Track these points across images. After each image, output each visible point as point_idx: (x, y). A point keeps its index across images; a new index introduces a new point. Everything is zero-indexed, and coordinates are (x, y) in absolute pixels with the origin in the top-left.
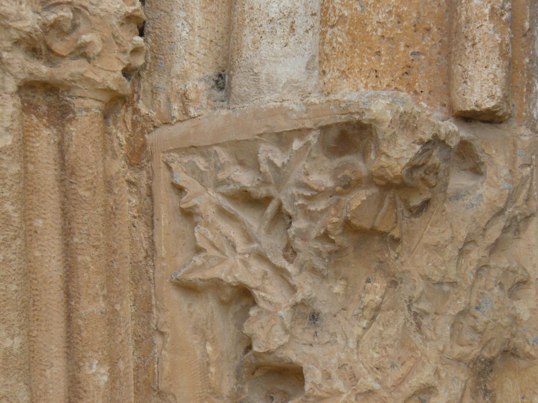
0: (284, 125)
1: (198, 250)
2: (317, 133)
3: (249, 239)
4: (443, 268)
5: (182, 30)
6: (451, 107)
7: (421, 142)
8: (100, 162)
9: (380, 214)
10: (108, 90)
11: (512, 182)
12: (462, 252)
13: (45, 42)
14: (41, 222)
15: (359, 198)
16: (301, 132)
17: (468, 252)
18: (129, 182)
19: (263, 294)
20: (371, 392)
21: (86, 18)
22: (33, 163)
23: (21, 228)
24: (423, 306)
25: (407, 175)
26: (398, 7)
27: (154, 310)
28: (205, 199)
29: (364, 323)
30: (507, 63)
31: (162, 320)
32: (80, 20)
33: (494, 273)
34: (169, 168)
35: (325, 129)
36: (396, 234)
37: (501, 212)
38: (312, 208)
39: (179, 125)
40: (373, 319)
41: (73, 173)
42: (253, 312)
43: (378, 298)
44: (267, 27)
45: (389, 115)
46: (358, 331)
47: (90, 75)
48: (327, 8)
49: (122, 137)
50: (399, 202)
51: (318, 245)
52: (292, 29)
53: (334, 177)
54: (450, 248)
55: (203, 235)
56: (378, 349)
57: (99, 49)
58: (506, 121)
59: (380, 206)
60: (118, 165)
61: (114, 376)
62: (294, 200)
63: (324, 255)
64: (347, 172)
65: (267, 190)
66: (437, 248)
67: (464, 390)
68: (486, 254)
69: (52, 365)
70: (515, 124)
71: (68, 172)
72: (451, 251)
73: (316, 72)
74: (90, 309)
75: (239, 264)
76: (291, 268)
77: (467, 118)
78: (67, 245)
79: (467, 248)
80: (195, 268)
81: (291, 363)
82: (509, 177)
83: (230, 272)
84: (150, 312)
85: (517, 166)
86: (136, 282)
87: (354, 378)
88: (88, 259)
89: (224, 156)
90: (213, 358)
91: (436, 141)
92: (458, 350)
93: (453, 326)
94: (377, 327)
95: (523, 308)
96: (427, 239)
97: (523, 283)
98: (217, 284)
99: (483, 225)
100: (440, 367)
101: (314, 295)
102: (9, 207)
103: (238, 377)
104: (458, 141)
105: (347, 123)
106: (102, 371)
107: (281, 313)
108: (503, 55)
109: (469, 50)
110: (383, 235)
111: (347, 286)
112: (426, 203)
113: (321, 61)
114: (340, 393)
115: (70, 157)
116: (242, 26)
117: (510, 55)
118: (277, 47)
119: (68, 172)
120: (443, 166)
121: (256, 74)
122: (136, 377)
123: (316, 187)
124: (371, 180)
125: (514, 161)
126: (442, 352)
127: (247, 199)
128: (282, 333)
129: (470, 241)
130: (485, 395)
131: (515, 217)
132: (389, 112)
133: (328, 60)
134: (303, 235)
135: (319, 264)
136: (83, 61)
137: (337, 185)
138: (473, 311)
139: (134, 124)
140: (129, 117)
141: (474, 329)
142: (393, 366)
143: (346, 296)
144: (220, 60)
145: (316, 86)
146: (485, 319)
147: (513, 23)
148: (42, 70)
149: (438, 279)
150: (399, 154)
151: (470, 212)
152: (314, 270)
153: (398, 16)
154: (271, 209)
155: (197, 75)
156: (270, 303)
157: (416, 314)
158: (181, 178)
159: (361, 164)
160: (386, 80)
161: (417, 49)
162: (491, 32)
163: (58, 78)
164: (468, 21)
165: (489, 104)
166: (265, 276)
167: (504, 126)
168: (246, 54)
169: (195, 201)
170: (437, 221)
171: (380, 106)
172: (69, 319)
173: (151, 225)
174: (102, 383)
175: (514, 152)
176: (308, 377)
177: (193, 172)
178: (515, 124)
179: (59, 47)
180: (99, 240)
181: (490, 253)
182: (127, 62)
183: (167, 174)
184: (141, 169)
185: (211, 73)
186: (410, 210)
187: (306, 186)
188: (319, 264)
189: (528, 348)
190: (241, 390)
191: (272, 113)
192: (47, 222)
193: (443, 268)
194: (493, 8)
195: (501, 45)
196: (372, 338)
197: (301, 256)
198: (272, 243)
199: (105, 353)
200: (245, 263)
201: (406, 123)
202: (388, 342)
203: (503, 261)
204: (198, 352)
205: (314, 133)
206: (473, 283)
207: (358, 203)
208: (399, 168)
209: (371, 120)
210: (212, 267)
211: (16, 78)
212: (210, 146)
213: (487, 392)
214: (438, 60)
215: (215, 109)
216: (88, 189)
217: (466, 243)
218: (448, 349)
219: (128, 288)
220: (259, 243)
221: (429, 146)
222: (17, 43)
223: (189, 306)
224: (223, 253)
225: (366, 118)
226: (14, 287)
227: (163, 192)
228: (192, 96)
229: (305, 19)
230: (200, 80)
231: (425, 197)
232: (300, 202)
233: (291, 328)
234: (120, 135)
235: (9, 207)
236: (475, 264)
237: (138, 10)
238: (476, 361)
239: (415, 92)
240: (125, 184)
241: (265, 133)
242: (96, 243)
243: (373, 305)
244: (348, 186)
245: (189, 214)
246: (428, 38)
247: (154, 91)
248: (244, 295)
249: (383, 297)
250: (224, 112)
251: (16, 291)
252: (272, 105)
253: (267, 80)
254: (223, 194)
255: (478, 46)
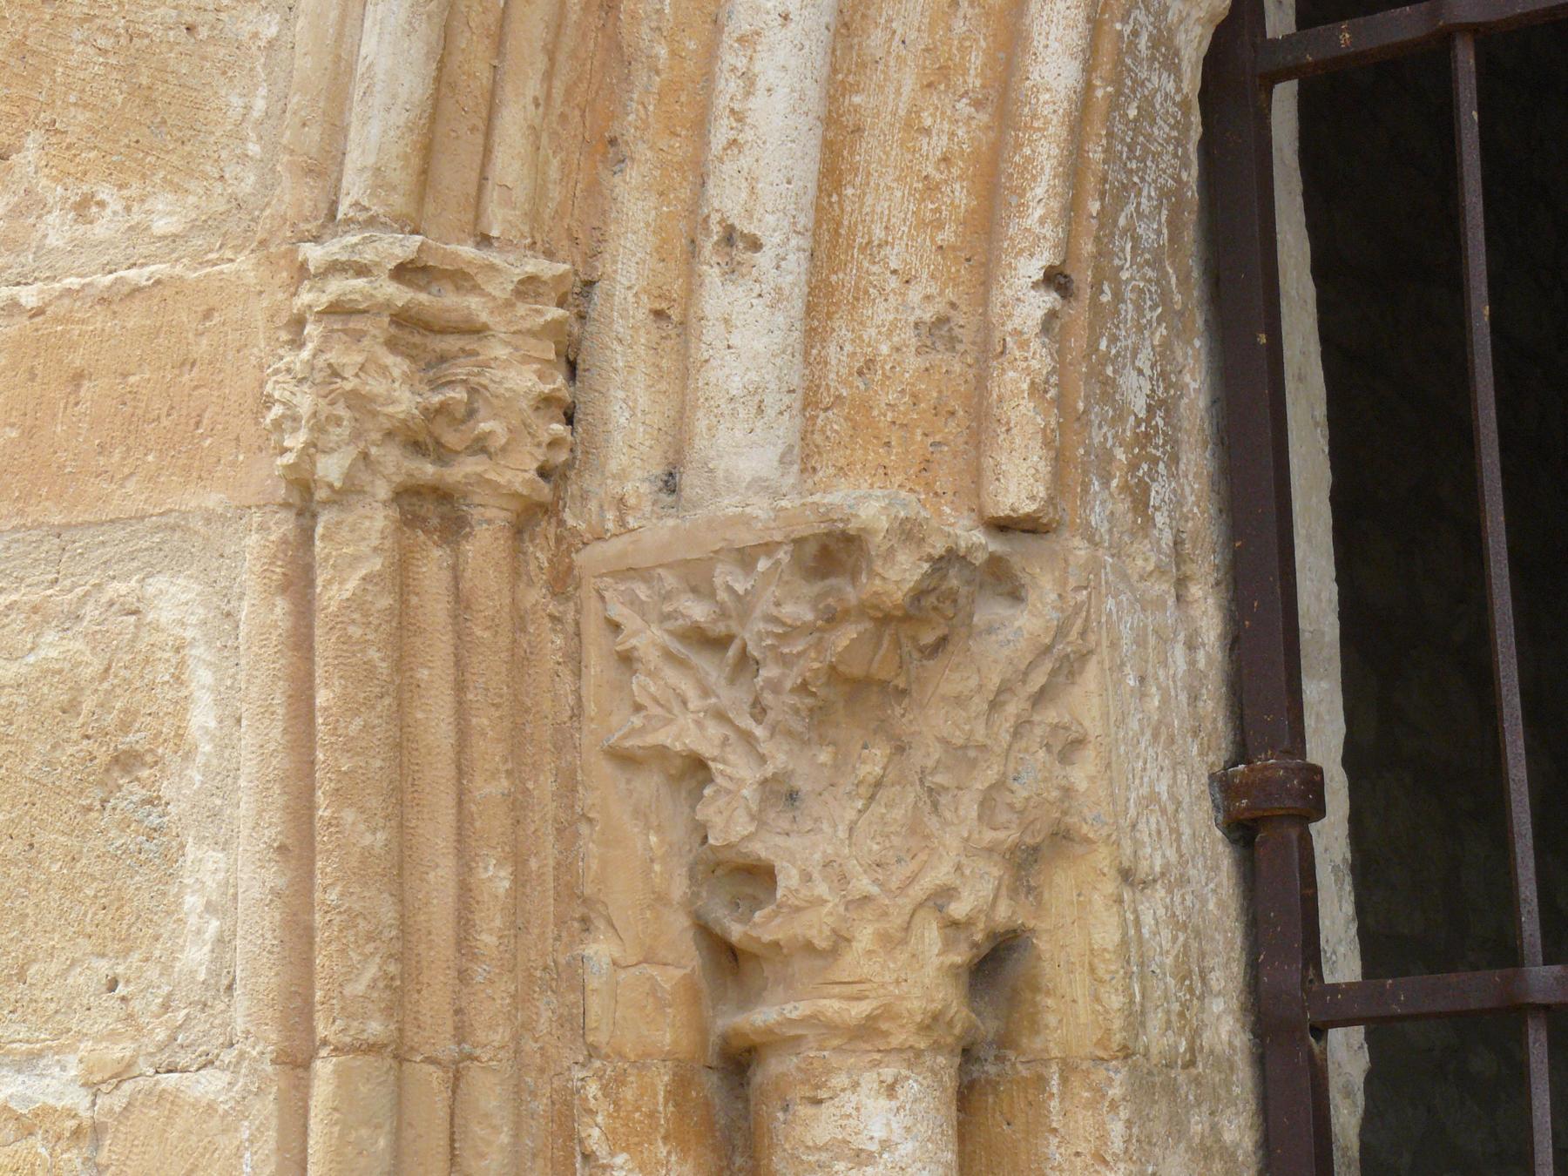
0: (747, 538)
1: (638, 708)
2: (789, 548)
3: (706, 692)
4: (967, 727)
5: (619, 416)
6: (981, 512)
7: (930, 558)
8: (506, 592)
9: (878, 658)
10: (515, 495)
11: (1062, 610)
12: (995, 705)
13: (430, 434)
14: (426, 672)
15: (845, 637)
16: (768, 548)
17: (1004, 703)
18: (552, 617)
19: (721, 767)
20: (867, 899)
21: (486, 400)
22: (417, 594)
23: (392, 682)
24: (939, 779)
25: (912, 604)
26: (913, 385)
27: (580, 788)
28: (647, 638)
29: (860, 804)
30: (1052, 454)
31: (589, 802)
32: (479, 404)
33: (1038, 731)
34: (602, 598)
35: (799, 542)
36: (901, 683)
37: (1048, 649)
38: (786, 650)
39: (614, 540)
40: (872, 797)
41: (468, 607)
42: (708, 791)
43: (878, 770)
44: (726, 408)
45: (884, 524)
46: (850, 815)
47: (491, 476)
48: (818, 386)
49: (543, 557)
50: (904, 640)
51: (793, 700)
52: (760, 410)
53: (815, 608)
54: (976, 699)
55: (644, 688)
56: (879, 839)
57: (503, 441)
58: (1055, 530)
59: (878, 645)
60: (535, 596)
61: (520, 880)
62: (761, 640)
63: (803, 714)
64: (831, 601)
65: (728, 626)
66: (959, 701)
67: (998, 888)
68: (1027, 705)
69: (437, 866)
70: (1067, 535)
71: (463, 605)
72: (979, 704)
73: (796, 468)
74: (486, 790)
75: (692, 726)
76: (759, 732)
77: (1002, 526)
78: (460, 703)
79: (1002, 698)
80: (633, 732)
81: (759, 859)
82: (1058, 604)
83: (677, 738)
84: (574, 790)
85: (1069, 588)
86: (559, 749)
87: (844, 879)
88: (486, 722)
89: (670, 581)
90: (659, 853)
91: (952, 558)
92: (989, 836)
93: (982, 804)
94: (878, 809)
95: (1081, 774)
96: (948, 689)
97: (1079, 742)
98: (662, 752)
99: (1023, 667)
100: (964, 860)
101: (791, 767)
102: (373, 654)
103: (692, 876)
104: (986, 556)
105: (828, 534)
106: (502, 874)
107: (745, 792)
108: (1047, 444)
109: (1002, 437)
110: (883, 684)
111: (836, 753)
112: (943, 642)
113: (805, 456)
114: (824, 902)
115: (465, 585)
116: (695, 408)
117: (1057, 444)
118: (738, 434)
119: (463, 605)
120: (964, 590)
121: (711, 471)
122: (556, 879)
123: (789, 621)
124: (863, 610)
125: (1065, 584)
126: (967, 840)
127: (711, 642)
128: (747, 819)
129: (1005, 689)
130: (1028, 893)
131: (1067, 656)
132: (884, 518)
133: (820, 453)
134: (775, 687)
135: (798, 726)
136: (483, 457)
137: (817, 619)
138: (1010, 782)
139: (559, 540)
140: (552, 531)
141: (1011, 806)
142: (899, 861)
143: (836, 767)
144: (670, 455)
145: (794, 486)
146: (1025, 794)
147: (1061, 402)
148: (428, 470)
149: (961, 742)
150: (900, 574)
151: (1006, 651)
152: (790, 733)
153: (914, 395)
154: (732, 652)
155: (639, 474)
156: (731, 778)
157: (930, 790)
158: (618, 611)
159: (849, 589)
160: (899, 478)
161: (938, 438)
162: (1031, 414)
163: (450, 480)
164: (1000, 399)
165: (1028, 507)
166: (725, 741)
167: (1051, 536)
168: (699, 443)
169: (634, 642)
170: (959, 664)
171: (869, 504)
172: (460, 803)
173: (578, 674)
174: (501, 891)
175: (1065, 570)
176: (780, 878)
177: (632, 603)
178: (1067, 535)
179: (451, 438)
180: (501, 696)
181: (1034, 705)
182: (542, 458)
183: (599, 605)
184: (568, 599)
185: (659, 471)
186: (921, 650)
187: (776, 620)
188: (798, 726)
189: (1085, 829)
190: (696, 895)
191: (733, 521)
192: (435, 673)
193: (967, 727)
194: (1033, 383)
195: (1044, 430)
196: (870, 824)
197: (771, 715)
198: (733, 698)
199: (507, 849)
200: (698, 723)
201: (909, 532)
202: (892, 829)
203: (1051, 715)
204: (639, 845)
205: (786, 548)
206: (1010, 746)
207: (846, 642)
208: (900, 595)
209: (860, 529)
210: (655, 730)
211: (389, 481)
212: (653, 568)
213: (1030, 889)
214: (965, 452)
215: (660, 518)
216: (488, 628)
217: (999, 692)
218: (976, 836)
219: (548, 758)
220: (718, 697)
221: (943, 564)
222: (389, 434)
223: (628, 781)
224: (670, 711)
225: (852, 528)
226: (379, 763)
227: (593, 629)
228: (632, 501)
229: (778, 397)
230: (644, 480)
231: (939, 632)
232: (769, 642)
233: (760, 811)
234: (539, 555)
235: (373, 654)
236: (1012, 720)
237: (559, 390)
238: (1016, 847)
239: (936, 494)
240: (547, 620)
241: (721, 549)
242: (497, 701)
243: (871, 779)
244: (832, 619)
245: (627, 660)
246: (952, 424)
247: (584, 496)
248: (696, 769)
249: (885, 768)
250: (671, 522)
251: (381, 768)
252: (731, 511)
253: (726, 478)
254: (671, 633)
255: (1014, 431)
